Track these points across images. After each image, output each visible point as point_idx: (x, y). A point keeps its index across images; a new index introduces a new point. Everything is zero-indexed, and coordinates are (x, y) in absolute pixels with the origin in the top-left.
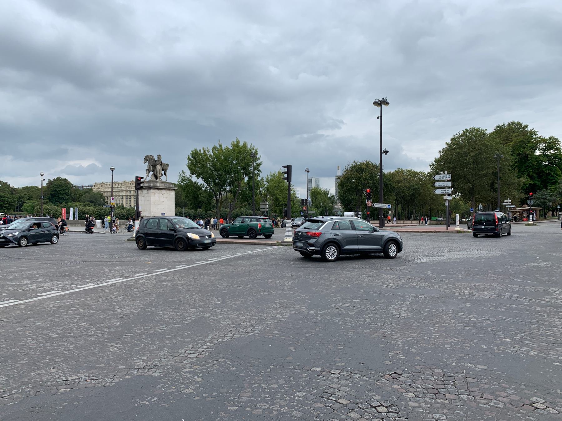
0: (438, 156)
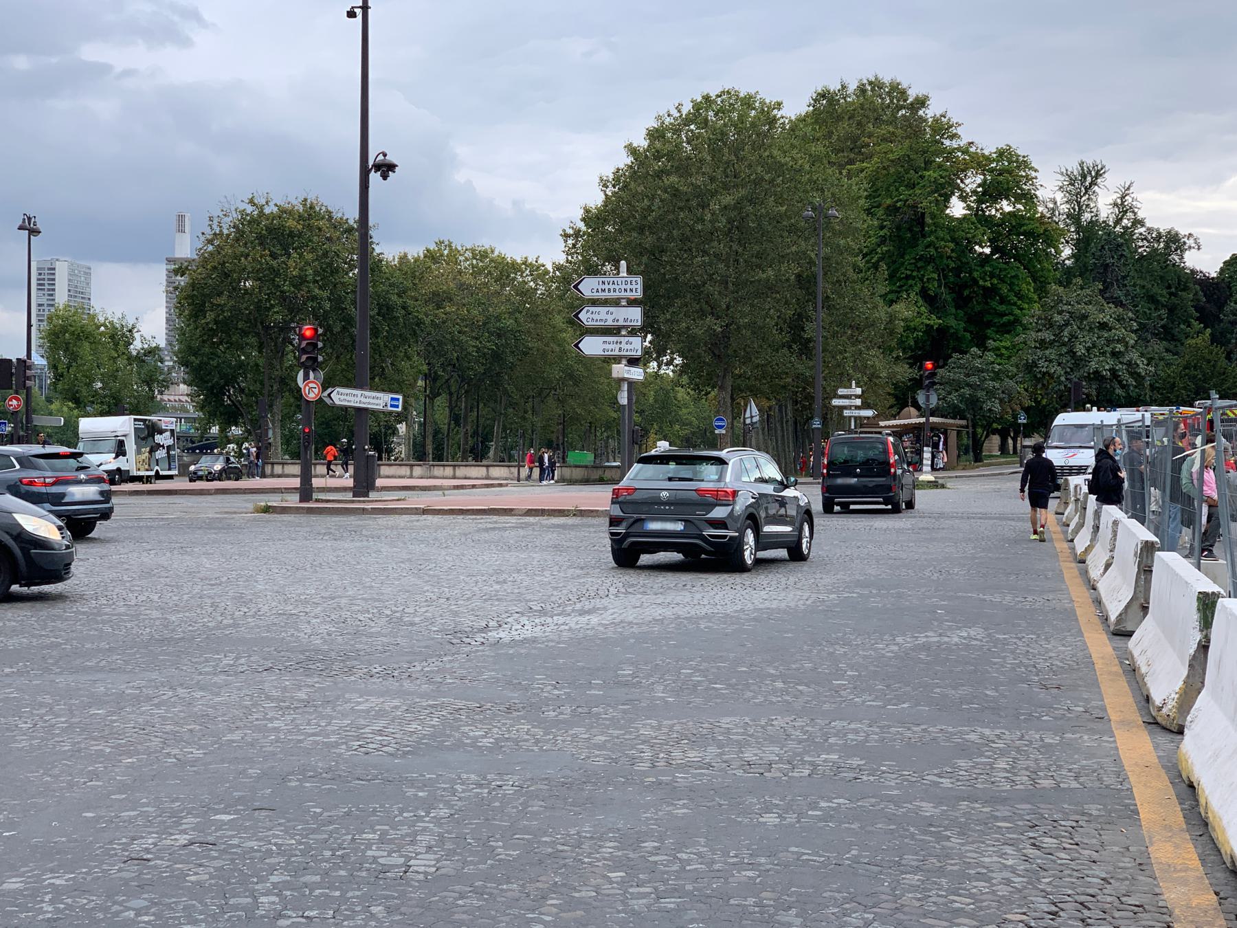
0: (596, 199)
